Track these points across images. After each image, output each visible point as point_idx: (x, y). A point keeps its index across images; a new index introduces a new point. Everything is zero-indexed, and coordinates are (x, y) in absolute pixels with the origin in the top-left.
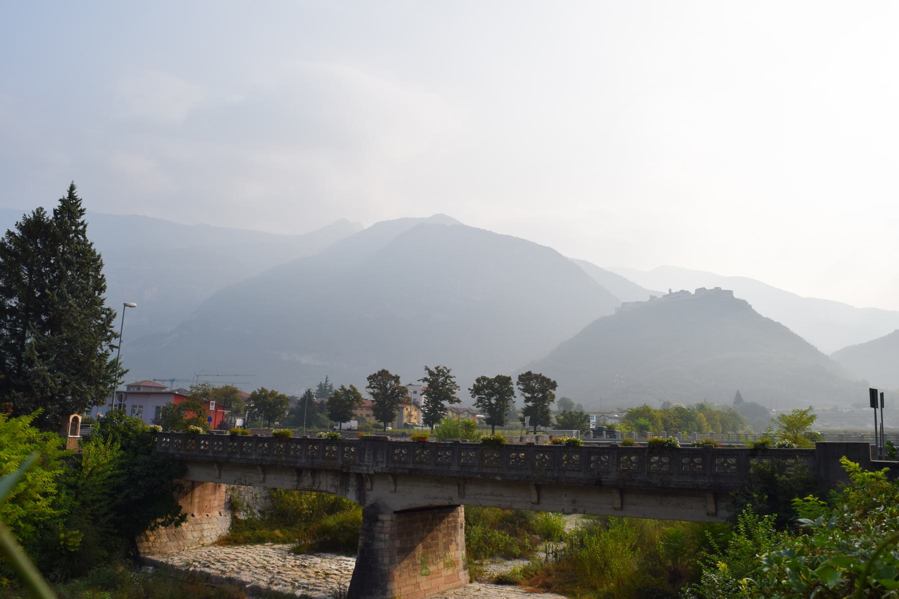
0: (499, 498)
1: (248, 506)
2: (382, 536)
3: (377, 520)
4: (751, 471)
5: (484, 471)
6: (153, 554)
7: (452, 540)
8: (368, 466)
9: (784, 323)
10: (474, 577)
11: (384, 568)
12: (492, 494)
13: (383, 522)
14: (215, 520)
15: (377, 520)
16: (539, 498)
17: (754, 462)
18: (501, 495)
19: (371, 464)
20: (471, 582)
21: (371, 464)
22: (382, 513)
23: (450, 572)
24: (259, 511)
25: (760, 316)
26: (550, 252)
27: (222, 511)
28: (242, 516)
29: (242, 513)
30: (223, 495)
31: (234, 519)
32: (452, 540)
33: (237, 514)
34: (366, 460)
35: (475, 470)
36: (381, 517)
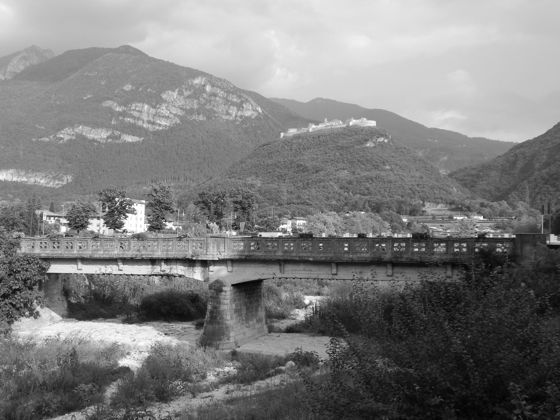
0: (309, 272)
1: (75, 293)
2: (225, 301)
3: (221, 291)
4: (477, 250)
5: (301, 255)
6: (484, 229)
7: (259, 305)
8: (213, 255)
9: (357, 104)
10: (271, 330)
11: (227, 322)
12: (304, 270)
13: (226, 292)
14: (56, 304)
15: (221, 291)
16: (337, 271)
17: (477, 245)
18: (311, 270)
19: (215, 253)
20: (270, 332)
21: (215, 253)
22: (225, 286)
23: (260, 326)
24: (82, 297)
25: (425, 127)
26: (375, 109)
27: (59, 297)
28: (73, 301)
29: (72, 298)
30: (60, 285)
31: (69, 303)
32: (259, 305)
33: (69, 299)
34: (211, 250)
35: (294, 254)
36: (224, 289)
